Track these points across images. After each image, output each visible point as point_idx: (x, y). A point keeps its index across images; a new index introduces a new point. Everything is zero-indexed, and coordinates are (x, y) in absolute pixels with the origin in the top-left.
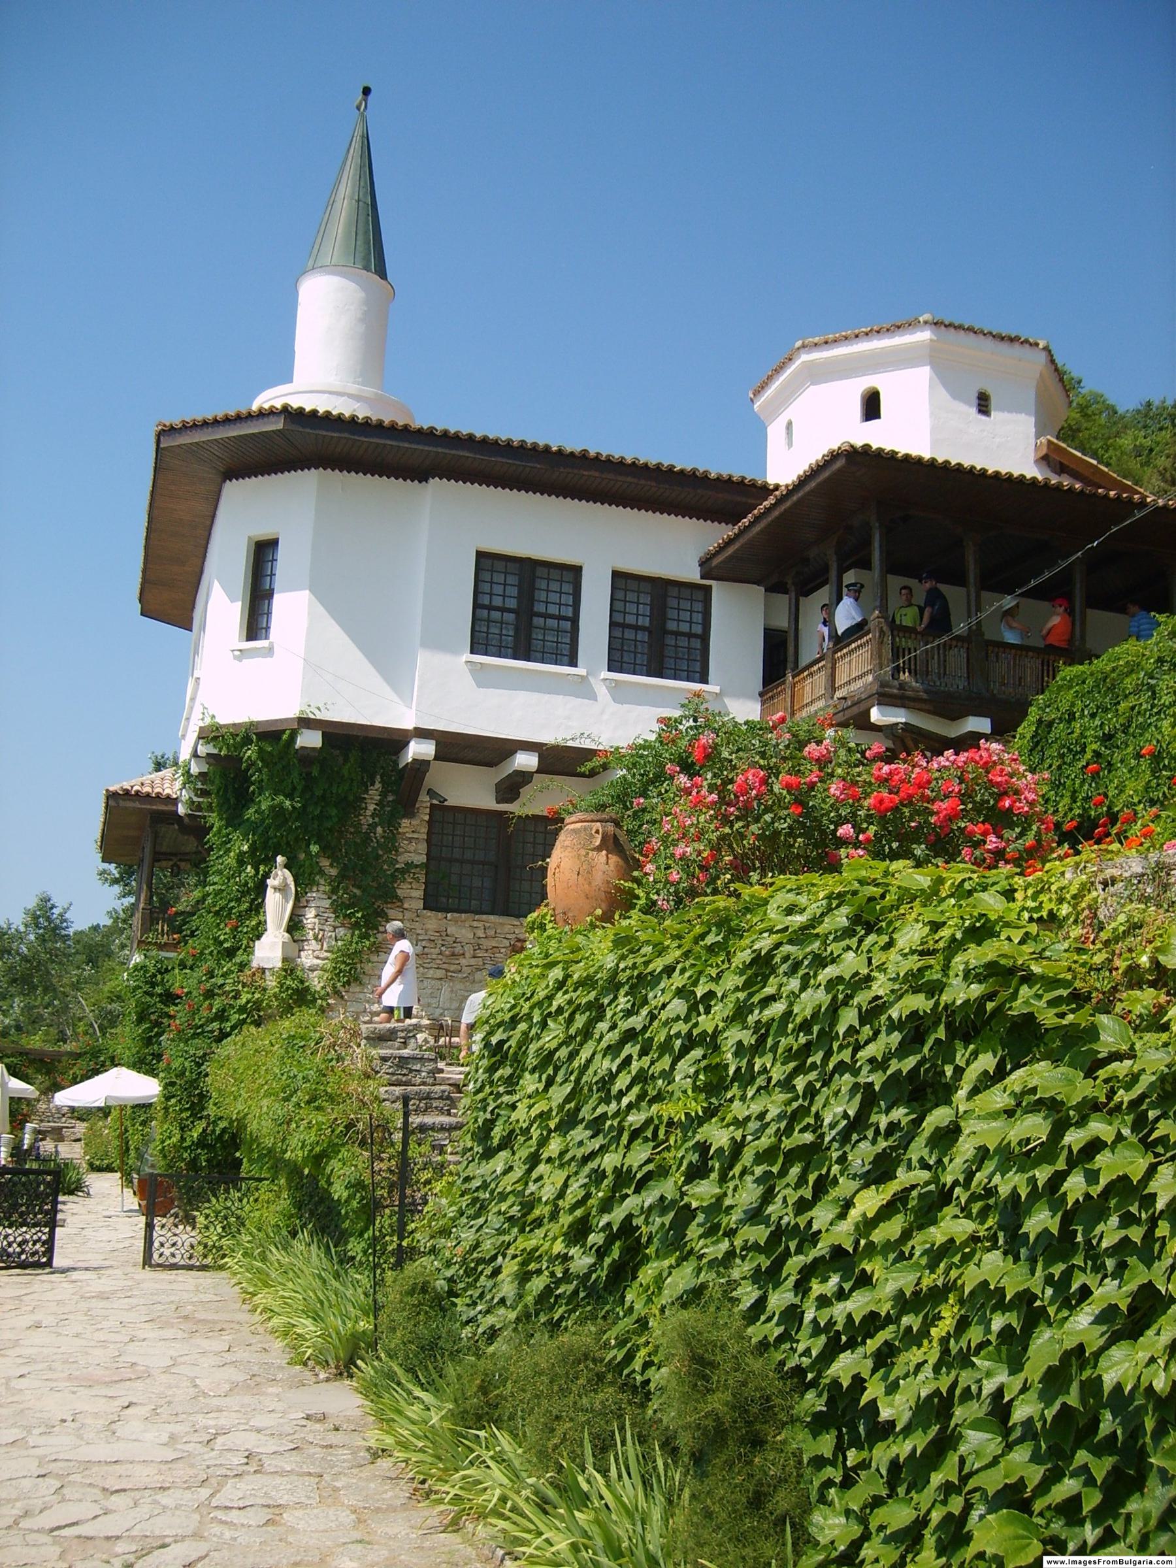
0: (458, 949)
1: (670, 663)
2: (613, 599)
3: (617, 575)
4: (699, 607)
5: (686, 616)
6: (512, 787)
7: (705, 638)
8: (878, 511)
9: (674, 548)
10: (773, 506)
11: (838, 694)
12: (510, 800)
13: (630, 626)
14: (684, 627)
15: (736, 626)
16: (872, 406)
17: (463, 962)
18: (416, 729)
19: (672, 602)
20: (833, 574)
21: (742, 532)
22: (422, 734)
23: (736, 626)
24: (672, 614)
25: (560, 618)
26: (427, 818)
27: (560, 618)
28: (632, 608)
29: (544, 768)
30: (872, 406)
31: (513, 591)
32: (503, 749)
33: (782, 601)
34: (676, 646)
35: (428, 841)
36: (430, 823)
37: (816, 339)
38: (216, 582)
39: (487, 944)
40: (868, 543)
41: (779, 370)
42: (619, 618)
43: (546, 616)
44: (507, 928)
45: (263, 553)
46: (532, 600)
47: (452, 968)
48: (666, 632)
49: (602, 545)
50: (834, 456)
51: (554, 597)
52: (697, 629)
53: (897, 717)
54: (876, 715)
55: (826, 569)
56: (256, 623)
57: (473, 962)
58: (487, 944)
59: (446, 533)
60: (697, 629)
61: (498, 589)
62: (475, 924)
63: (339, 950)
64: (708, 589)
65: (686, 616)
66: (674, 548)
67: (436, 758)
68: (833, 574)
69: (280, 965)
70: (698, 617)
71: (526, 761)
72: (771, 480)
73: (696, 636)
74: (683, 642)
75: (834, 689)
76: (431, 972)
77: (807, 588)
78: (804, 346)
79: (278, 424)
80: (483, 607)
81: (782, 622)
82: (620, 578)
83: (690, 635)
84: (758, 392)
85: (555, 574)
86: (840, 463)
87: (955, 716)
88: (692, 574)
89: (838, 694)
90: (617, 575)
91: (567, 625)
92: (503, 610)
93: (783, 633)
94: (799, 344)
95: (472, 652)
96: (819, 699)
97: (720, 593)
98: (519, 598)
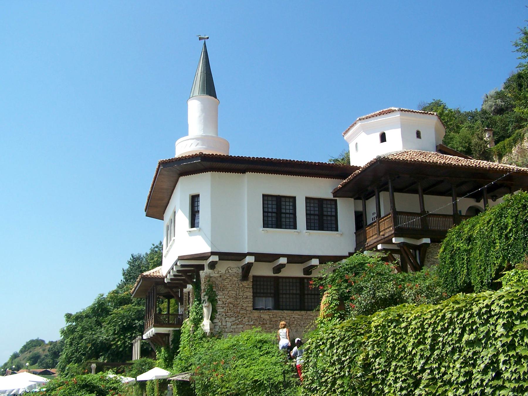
0: (265, 322)
1: (325, 225)
3: (307, 199)
4: (333, 206)
6: (278, 269)
8: (387, 175)
9: (323, 188)
11: (381, 234)
12: (278, 273)
13: (312, 215)
14: (329, 213)
17: (267, 326)
19: (325, 206)
20: (376, 193)
24: (325, 209)
30: (383, 138)
31: (274, 206)
33: (360, 202)
34: (327, 220)
35: (253, 288)
36: (252, 282)
37: (364, 117)
38: (180, 210)
41: (353, 126)
42: (266, 210)
44: (280, 314)
45: (194, 199)
46: (281, 209)
48: (324, 215)
49: (302, 190)
53: (401, 240)
57: (270, 326)
58: (273, 319)
59: (252, 189)
60: (334, 214)
61: (270, 206)
64: (336, 201)
66: (323, 188)
68: (376, 193)
70: (333, 210)
72: (353, 163)
73: (333, 216)
74: (329, 218)
75: (380, 232)
78: (360, 120)
80: (266, 212)
81: (360, 209)
83: (331, 216)
84: (347, 132)
85: (287, 200)
87: (419, 238)
88: (331, 197)
90: (307, 199)
91: (292, 216)
92: (272, 213)
94: (358, 119)
96: (375, 235)
98: (277, 208)
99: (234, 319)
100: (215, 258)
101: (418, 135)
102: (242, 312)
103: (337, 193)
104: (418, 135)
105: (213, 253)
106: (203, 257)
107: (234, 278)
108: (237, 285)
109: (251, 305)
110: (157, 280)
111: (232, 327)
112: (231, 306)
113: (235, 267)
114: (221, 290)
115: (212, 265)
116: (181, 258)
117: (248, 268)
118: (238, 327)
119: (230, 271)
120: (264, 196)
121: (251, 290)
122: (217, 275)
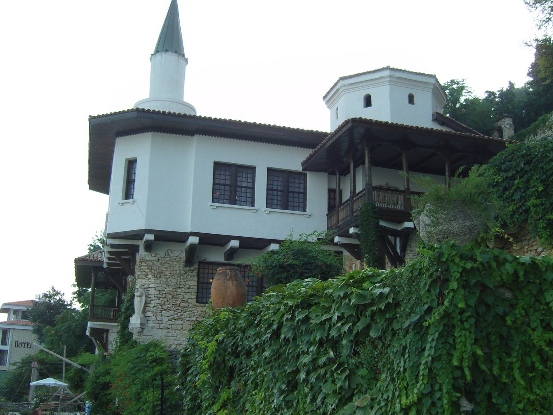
5: (297, 185)
7: (305, 193)
10: (327, 142)
11: (355, 215)
15: (316, 190)
16: (368, 102)
18: (191, 232)
21: (316, 152)
22: (193, 234)
23: (316, 190)
26: (197, 267)
29: (241, 246)
30: (368, 102)
40: (363, 156)
42: (270, 187)
45: (131, 164)
46: (236, 181)
48: (289, 192)
49: (263, 160)
50: (347, 122)
52: (302, 190)
54: (337, 239)
55: (349, 167)
59: (196, 160)
65: (297, 185)
66: (292, 160)
69: (139, 326)
70: (302, 186)
71: (235, 243)
77: (344, 172)
81: (334, 186)
82: (271, 171)
83: (299, 193)
86: (350, 125)
87: (401, 222)
89: (355, 215)
95: (213, 202)
97: (310, 177)
99: (172, 313)
100: (151, 237)
101: (411, 99)
102: (182, 305)
103: (310, 165)
104: (411, 99)
106: (138, 235)
107: (175, 263)
108: (178, 272)
109: (195, 297)
110: (94, 265)
111: (169, 322)
112: (170, 296)
113: (179, 252)
114: (158, 276)
115: (149, 247)
118: (177, 322)
119: (170, 254)
121: (196, 278)
122: (154, 259)
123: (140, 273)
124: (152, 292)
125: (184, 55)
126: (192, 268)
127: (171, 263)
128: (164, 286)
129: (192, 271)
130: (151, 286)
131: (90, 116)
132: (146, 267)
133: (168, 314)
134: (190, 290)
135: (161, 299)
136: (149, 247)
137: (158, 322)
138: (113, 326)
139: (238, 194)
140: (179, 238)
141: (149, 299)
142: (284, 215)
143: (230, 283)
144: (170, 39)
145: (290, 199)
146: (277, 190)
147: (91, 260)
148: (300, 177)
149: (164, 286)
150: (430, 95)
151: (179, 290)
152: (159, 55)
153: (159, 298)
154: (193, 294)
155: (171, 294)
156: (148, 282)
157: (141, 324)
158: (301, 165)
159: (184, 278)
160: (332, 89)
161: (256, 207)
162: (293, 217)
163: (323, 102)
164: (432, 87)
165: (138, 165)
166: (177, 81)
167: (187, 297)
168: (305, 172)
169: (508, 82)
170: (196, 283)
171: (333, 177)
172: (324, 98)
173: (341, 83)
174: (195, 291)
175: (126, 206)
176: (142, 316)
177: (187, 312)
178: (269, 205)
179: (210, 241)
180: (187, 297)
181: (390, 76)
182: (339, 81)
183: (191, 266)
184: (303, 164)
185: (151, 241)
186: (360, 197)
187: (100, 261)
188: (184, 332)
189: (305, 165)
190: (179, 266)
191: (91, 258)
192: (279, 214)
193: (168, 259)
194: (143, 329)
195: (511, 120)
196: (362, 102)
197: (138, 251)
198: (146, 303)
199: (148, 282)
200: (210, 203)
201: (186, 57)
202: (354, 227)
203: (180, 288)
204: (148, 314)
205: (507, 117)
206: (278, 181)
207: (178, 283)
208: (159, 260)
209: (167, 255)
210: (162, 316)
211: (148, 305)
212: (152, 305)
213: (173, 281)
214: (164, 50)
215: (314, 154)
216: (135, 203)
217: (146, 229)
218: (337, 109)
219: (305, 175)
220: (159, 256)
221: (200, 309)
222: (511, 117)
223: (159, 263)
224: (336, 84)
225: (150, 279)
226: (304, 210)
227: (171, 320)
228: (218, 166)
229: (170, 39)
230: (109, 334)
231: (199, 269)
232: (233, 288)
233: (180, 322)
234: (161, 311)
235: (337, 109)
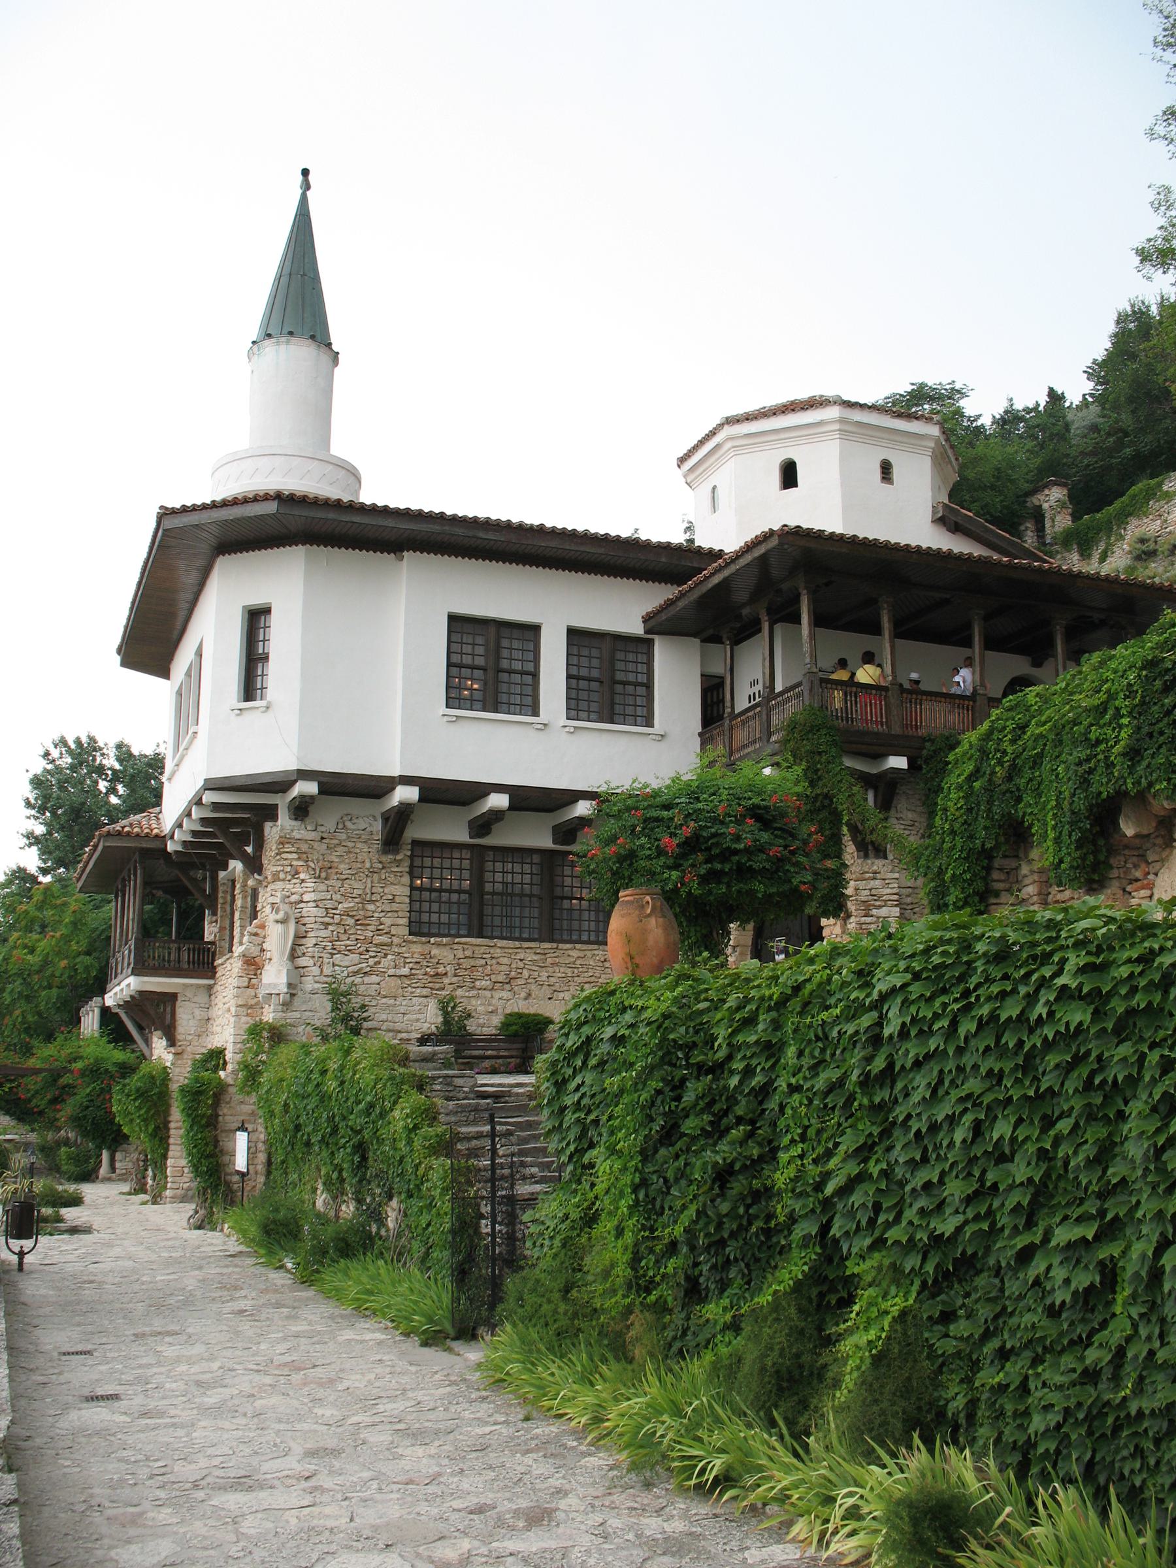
0: (441, 970)
2: (450, 642)
7: (649, 686)
9: (621, 609)
10: (712, 575)
15: (675, 679)
16: (789, 476)
17: (446, 981)
21: (682, 595)
23: (675, 679)
25: (522, 673)
26: (409, 853)
27: (522, 673)
28: (467, 649)
30: (789, 476)
31: (480, 650)
32: (472, 792)
39: (466, 964)
40: (796, 600)
42: (455, 659)
43: (510, 672)
45: (256, 618)
46: (498, 658)
47: (437, 986)
49: (556, 608)
51: (517, 655)
52: (642, 678)
56: (250, 689)
57: (455, 979)
58: (466, 964)
59: (407, 617)
62: (455, 947)
63: (57, 847)
66: (621, 609)
67: (421, 800)
69: (285, 990)
76: (418, 990)
79: (271, 507)
80: (455, 665)
81: (718, 669)
82: (576, 636)
86: (774, 542)
93: (721, 679)
100: (310, 788)
101: (886, 470)
103: (661, 624)
104: (886, 470)
105: (304, 775)
106: (279, 784)
107: (359, 845)
108: (368, 865)
109: (405, 921)
110: (145, 845)
112: (351, 921)
113: (368, 821)
114: (323, 875)
115: (301, 809)
116: (212, 785)
117: (401, 816)
118: (367, 979)
119: (348, 824)
120: (453, 619)
123: (280, 868)
124: (309, 910)
125: (330, 344)
126: (398, 857)
127: (350, 844)
128: (337, 897)
129: (398, 863)
130: (306, 898)
131: (161, 507)
132: (295, 856)
133: (346, 961)
134: (395, 906)
135: (331, 928)
136: (301, 809)
137: (326, 979)
138: (185, 986)
139: (504, 688)
140: (372, 788)
141: (304, 928)
142: (605, 736)
143: (653, 921)
144: (298, 306)
145: (618, 699)
146: (589, 680)
147: (138, 835)
148: (637, 648)
149: (337, 897)
150: (928, 462)
151: (371, 907)
152: (269, 347)
153: (326, 925)
154: (400, 914)
155: (352, 916)
156: (298, 889)
157: (290, 985)
158: (641, 620)
159: (380, 879)
160: (702, 442)
161: (544, 715)
162: (623, 741)
163: (678, 473)
164: (933, 445)
165: (275, 619)
166: (319, 412)
167: (388, 921)
168: (650, 636)
169: (1046, 391)
170: (407, 891)
171: (716, 647)
172: (682, 460)
173: (728, 431)
174: (406, 907)
175: (248, 717)
176: (289, 965)
177: (389, 957)
178: (573, 713)
179: (441, 794)
180: (388, 921)
181: (842, 421)
182: (720, 426)
183: (397, 852)
184: (646, 619)
185: (312, 797)
186: (788, 700)
187: (157, 836)
188: (384, 1000)
189: (652, 623)
190: (368, 854)
191: (136, 830)
192: (596, 734)
193: (344, 836)
194: (293, 995)
195: (1065, 492)
196: (776, 477)
197: (274, 818)
198: (297, 937)
199: (298, 889)
200: (443, 710)
201: (335, 348)
202: (772, 766)
203: (372, 901)
204: (302, 961)
205: (1055, 484)
206: (590, 657)
207: (368, 891)
208: (322, 838)
209: (340, 826)
210: (334, 965)
211: (303, 941)
212: (310, 942)
213: (357, 886)
214: (285, 331)
215: (678, 599)
216: (270, 710)
217: (299, 771)
218: (714, 488)
219: (650, 643)
220: (323, 829)
221: (417, 948)
222: (1064, 485)
223: (325, 846)
224: (713, 433)
225: (303, 881)
226: (649, 722)
227: (355, 973)
228: (455, 621)
229: (298, 306)
230: (178, 1004)
231: (412, 857)
232: (660, 931)
233: (375, 979)
234: (332, 954)
235: (714, 488)
